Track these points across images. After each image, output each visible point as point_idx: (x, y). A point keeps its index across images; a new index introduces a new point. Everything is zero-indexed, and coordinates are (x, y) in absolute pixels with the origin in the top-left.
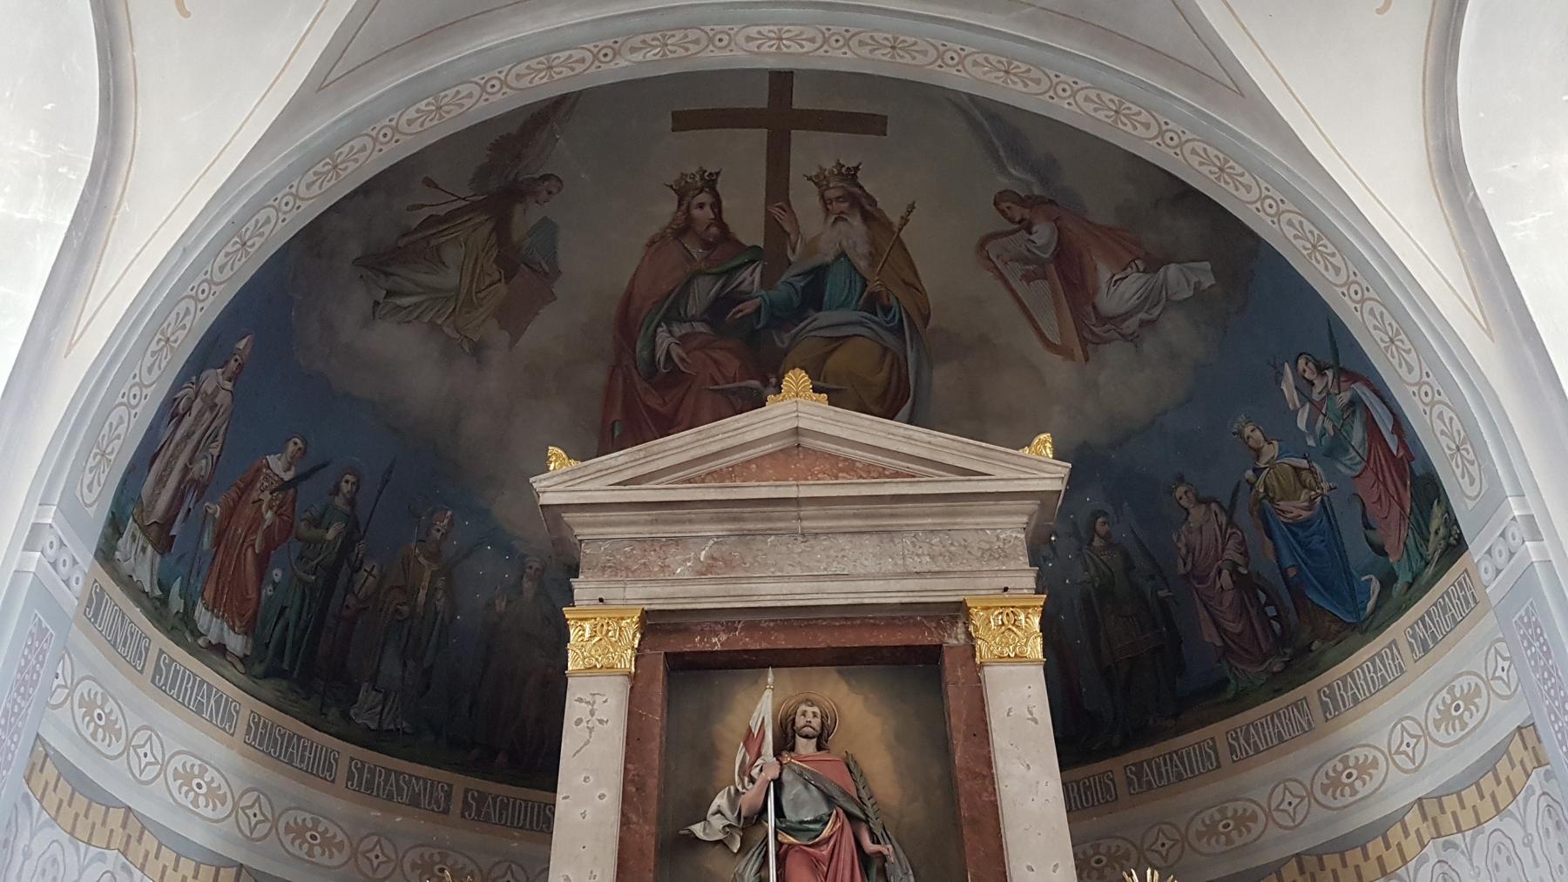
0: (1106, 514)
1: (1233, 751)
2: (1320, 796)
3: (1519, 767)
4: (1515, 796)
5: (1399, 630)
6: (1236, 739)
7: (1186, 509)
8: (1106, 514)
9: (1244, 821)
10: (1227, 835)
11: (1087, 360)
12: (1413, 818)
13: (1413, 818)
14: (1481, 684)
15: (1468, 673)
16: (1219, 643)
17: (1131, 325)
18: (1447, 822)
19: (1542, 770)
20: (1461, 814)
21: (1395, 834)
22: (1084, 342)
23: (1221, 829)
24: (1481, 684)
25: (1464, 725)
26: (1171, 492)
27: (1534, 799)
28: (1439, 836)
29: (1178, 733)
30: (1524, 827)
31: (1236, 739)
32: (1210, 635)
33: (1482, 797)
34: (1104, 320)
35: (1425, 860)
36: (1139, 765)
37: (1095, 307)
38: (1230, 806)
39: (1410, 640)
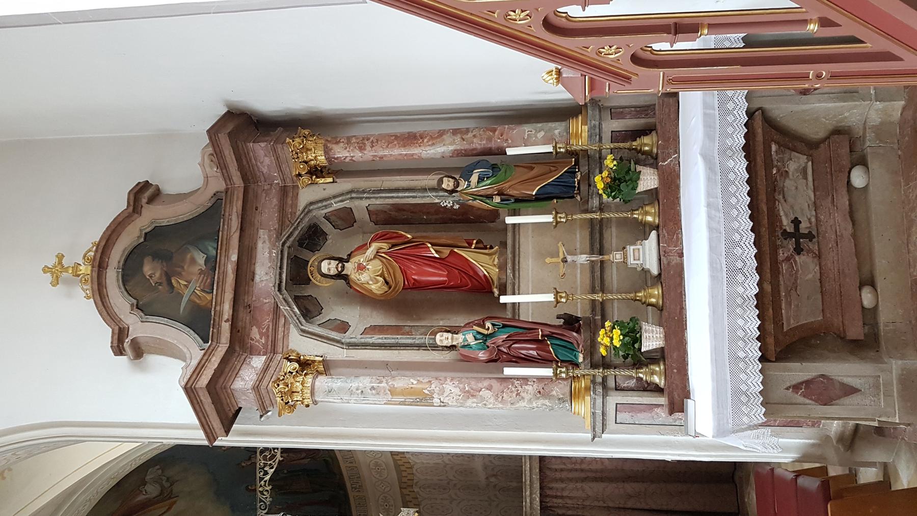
0: (247, 488)
1: (352, 463)
2: (382, 478)
3: (402, 459)
4: (417, 498)
5: (352, 495)
6: (347, 461)
7: (138, 308)
8: (247, 488)
9: (377, 464)
10: (381, 469)
11: (178, 496)
12: (406, 492)
13: (406, 492)
14: (384, 495)
15: (379, 497)
16: (309, 460)
17: (167, 485)
18: (410, 483)
19: (414, 486)
20: (409, 478)
21: (400, 463)
22: (170, 498)
23: (387, 507)
24: (384, 495)
25: (384, 469)
26: (243, 467)
27: (421, 493)
28: (412, 486)
29: (341, 474)
30: (425, 499)
31: (347, 461)
32: (306, 461)
33: (406, 471)
34: (161, 493)
35: (418, 492)
36: (352, 488)
37: (154, 498)
38: (371, 466)
39: (356, 490)
